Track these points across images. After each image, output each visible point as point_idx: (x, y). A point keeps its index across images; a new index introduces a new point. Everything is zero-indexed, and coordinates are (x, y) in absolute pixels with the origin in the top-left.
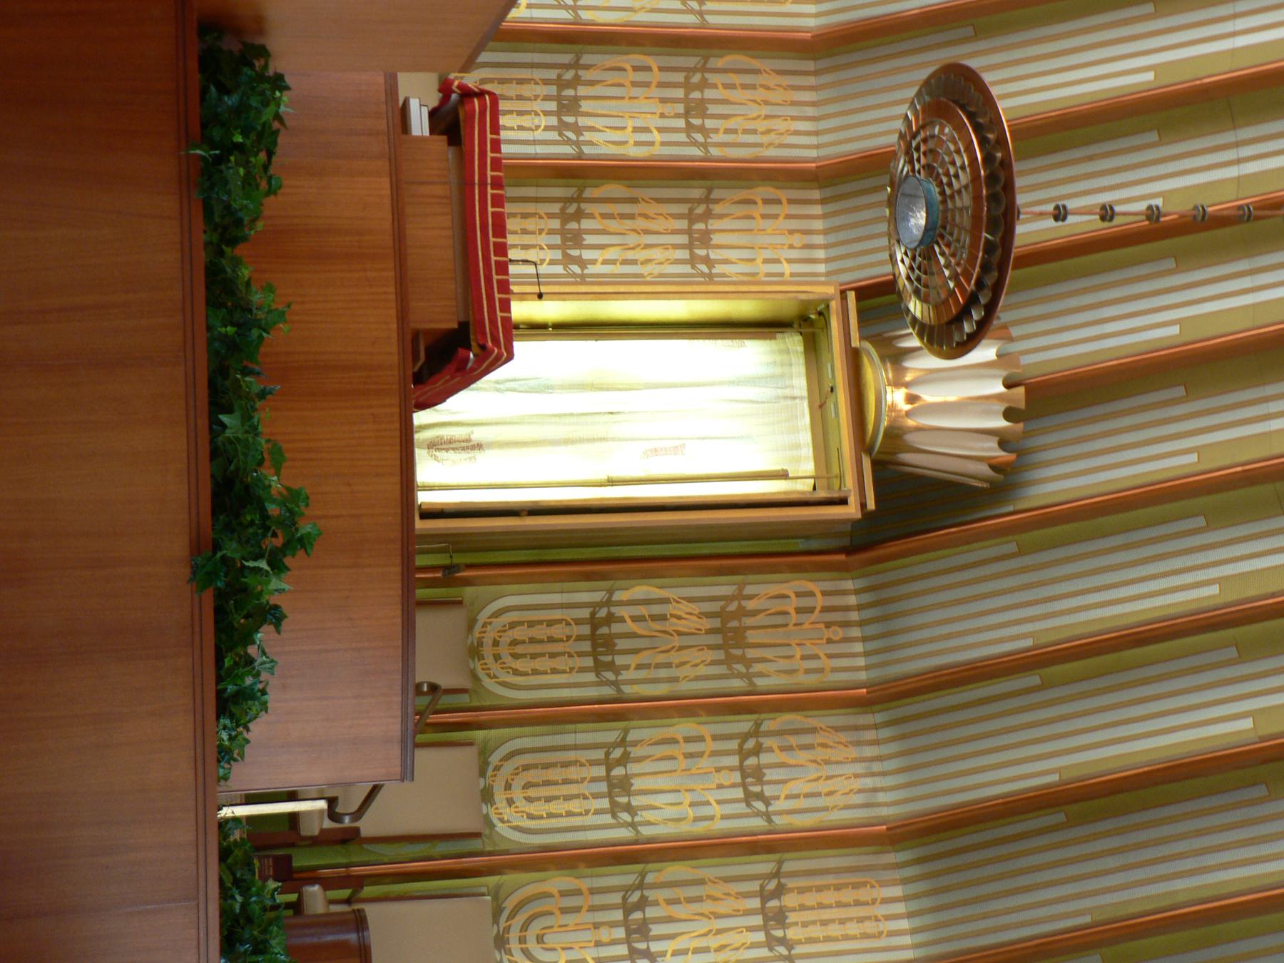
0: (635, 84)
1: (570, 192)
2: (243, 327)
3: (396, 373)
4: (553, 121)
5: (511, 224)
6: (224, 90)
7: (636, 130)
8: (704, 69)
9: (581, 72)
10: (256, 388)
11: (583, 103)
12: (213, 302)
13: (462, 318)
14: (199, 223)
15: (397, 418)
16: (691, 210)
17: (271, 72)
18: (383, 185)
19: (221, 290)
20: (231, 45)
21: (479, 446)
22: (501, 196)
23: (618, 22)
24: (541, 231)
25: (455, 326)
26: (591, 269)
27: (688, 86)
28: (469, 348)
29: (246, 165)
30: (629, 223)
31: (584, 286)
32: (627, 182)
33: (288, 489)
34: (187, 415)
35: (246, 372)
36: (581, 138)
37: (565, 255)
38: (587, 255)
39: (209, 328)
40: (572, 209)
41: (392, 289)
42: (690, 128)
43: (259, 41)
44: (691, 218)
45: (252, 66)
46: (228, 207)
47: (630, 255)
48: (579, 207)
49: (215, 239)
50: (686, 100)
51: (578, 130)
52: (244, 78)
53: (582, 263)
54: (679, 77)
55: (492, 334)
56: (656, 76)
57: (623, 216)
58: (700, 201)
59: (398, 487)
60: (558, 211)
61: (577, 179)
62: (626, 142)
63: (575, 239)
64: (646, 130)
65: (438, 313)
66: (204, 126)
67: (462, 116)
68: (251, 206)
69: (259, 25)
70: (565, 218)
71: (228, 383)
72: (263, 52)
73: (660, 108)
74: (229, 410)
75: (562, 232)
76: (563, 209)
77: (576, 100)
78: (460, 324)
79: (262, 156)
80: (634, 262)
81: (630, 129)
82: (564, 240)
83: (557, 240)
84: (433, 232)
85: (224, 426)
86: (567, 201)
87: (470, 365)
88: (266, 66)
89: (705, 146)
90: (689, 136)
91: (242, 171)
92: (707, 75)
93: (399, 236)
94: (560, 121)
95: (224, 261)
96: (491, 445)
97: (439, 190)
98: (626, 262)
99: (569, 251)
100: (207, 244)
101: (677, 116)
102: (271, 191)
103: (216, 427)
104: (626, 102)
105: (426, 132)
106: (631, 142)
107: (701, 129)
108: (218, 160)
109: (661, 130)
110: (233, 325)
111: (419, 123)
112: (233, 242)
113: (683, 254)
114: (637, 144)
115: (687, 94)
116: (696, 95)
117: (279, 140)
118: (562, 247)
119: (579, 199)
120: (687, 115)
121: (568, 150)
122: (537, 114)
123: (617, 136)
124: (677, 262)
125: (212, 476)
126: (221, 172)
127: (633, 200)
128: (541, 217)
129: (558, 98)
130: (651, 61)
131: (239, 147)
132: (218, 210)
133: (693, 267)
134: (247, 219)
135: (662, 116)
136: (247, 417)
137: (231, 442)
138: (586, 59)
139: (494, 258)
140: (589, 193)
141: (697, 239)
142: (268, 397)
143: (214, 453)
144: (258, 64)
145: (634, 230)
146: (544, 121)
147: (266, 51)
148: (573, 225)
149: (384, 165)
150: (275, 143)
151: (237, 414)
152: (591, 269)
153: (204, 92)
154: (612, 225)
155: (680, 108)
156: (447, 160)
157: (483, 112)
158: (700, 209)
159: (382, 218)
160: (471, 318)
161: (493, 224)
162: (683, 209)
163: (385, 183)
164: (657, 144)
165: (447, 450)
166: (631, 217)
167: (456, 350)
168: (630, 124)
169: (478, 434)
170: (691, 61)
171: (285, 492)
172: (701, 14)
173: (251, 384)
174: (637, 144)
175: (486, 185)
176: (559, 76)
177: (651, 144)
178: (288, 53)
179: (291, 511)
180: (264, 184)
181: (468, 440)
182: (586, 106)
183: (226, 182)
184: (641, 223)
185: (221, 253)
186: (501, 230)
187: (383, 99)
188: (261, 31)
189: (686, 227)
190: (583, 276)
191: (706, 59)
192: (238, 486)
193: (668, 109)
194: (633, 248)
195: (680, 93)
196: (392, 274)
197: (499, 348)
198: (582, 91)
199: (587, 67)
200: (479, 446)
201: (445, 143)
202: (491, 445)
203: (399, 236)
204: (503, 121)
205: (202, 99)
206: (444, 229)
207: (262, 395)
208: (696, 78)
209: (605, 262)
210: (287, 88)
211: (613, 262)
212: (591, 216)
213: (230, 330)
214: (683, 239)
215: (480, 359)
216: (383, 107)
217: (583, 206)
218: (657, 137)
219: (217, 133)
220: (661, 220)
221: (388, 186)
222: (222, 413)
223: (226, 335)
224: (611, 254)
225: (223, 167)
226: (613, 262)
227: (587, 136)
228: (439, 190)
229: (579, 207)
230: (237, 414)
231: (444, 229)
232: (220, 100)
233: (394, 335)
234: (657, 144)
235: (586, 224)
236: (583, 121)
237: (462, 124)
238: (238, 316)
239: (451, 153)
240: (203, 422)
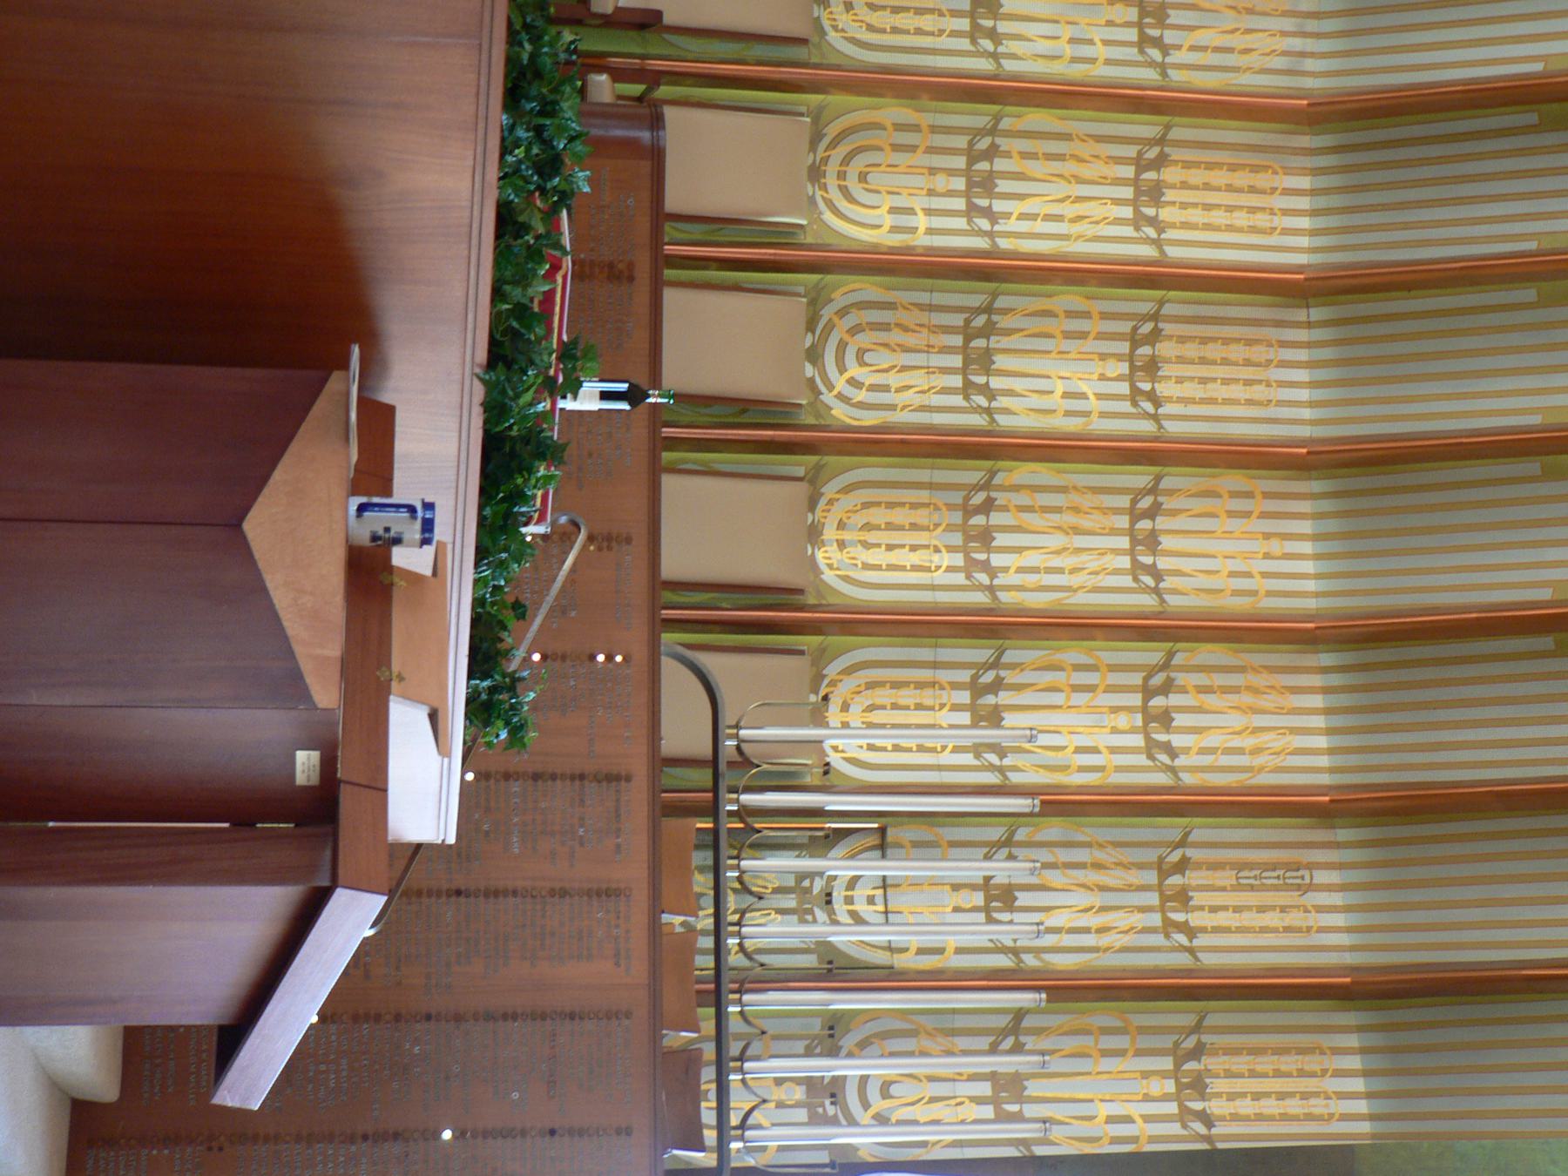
38: (999, 206)
51: (991, 394)
57: (1050, 157)
114: (1068, 413)
174: (1068, 413)
177: (1093, 61)
227: (1003, 402)
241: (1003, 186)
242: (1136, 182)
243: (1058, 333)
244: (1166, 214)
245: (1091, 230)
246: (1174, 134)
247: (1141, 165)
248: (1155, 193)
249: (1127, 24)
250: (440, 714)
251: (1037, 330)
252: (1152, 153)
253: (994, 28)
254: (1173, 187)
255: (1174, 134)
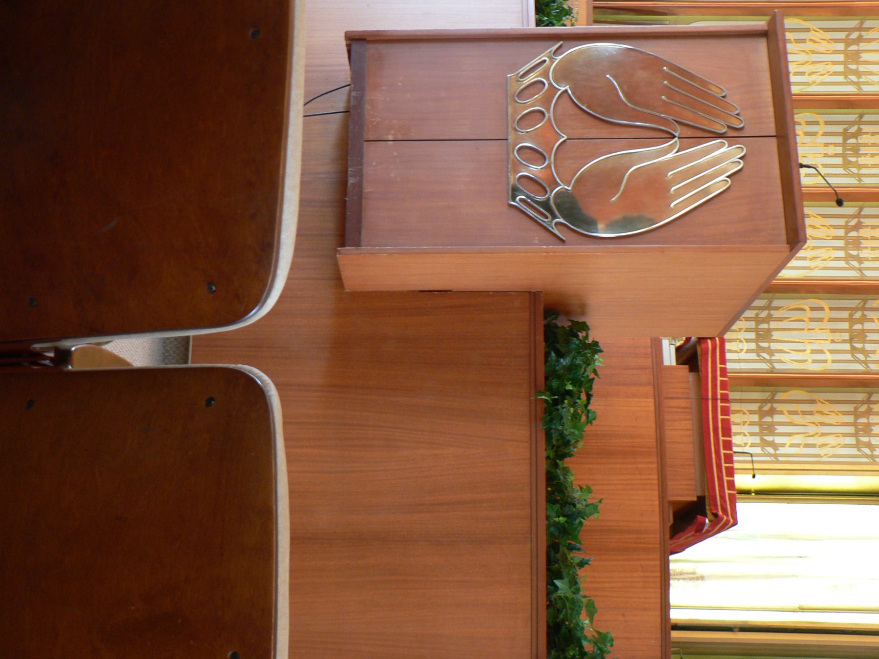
0: (812, 320)
1: (766, 395)
2: (571, 517)
3: (658, 536)
4: (753, 346)
5: (734, 429)
6: (560, 355)
7: (813, 352)
8: (863, 309)
9: (772, 312)
10: (577, 560)
11: (774, 333)
12: (551, 500)
13: (699, 494)
14: (542, 444)
15: (658, 569)
16: (856, 409)
17: (590, 341)
18: (649, 404)
19: (556, 491)
20: (563, 322)
21: (702, 578)
22: (728, 408)
23: (799, 277)
24: (744, 423)
25: (695, 499)
26: (781, 451)
27: (851, 320)
28: (705, 516)
29: (574, 405)
30: (810, 418)
31: (778, 465)
32: (809, 389)
33: (598, 633)
34: (532, 580)
35: (571, 548)
36: (773, 358)
37: (763, 440)
38: (778, 440)
39: (548, 518)
40: (767, 407)
41: (655, 477)
42: (854, 350)
43: (581, 319)
44: (856, 414)
45: (577, 336)
46: (561, 434)
47: (811, 441)
48: (772, 406)
49: (552, 455)
50: (850, 330)
51: (771, 352)
52: (574, 346)
53: (775, 446)
54: (845, 314)
55: (722, 506)
56: (827, 314)
57: (804, 413)
58: (863, 403)
59: (659, 619)
60: (756, 409)
61: (771, 385)
62: (806, 361)
63: (769, 429)
64: (821, 352)
65: (685, 491)
66: (546, 379)
67: (699, 353)
68: (577, 432)
69: (583, 308)
70: (762, 414)
71: (558, 556)
72: (584, 327)
73: (830, 336)
74: (560, 577)
75: (760, 424)
76: (760, 408)
77: (769, 331)
78: (698, 497)
79: (583, 397)
80: (813, 446)
81: (809, 351)
82: (762, 429)
83: (756, 429)
84: (681, 432)
85: (556, 588)
86: (764, 402)
87: (706, 528)
88: (587, 337)
89: (865, 362)
90: (853, 356)
91: (572, 410)
92: (866, 313)
93: (661, 440)
94: (758, 346)
95: (558, 471)
96: (710, 577)
97: (682, 403)
98: (807, 446)
99: (765, 438)
100: (548, 458)
101: (844, 341)
102: (589, 422)
103: (552, 588)
104: (806, 332)
105: (674, 363)
106: (810, 360)
107: (863, 351)
108: (556, 403)
109: (832, 352)
110: (564, 516)
111: (669, 357)
112: (562, 456)
113: (852, 441)
114: (814, 361)
115: (851, 326)
116: (858, 327)
117: (594, 386)
118: (760, 434)
119: (772, 401)
120: (851, 341)
121: (764, 366)
122: (741, 341)
123: (800, 356)
124: (846, 446)
125: (547, 622)
126: (558, 410)
127: (812, 402)
128: (744, 413)
129: (756, 330)
130: (822, 303)
131: (569, 393)
132: (555, 436)
133: (859, 450)
134: (573, 441)
135: (833, 341)
136: (573, 582)
137: (560, 598)
138: (776, 303)
139: (722, 452)
140: (780, 396)
141: (861, 430)
142: (586, 566)
143: (550, 605)
144: (581, 335)
145: (813, 423)
146: (746, 346)
147: (587, 326)
148: (768, 419)
149: (650, 390)
150: (591, 388)
151: (566, 580)
152: (781, 451)
153: (547, 355)
154: (797, 419)
155: (846, 336)
156: (688, 382)
157: (714, 349)
158: (863, 408)
159: (648, 426)
160: (707, 494)
161: (723, 428)
162: (850, 408)
163: (651, 402)
164: (829, 361)
165: (679, 579)
166: (811, 413)
167: (696, 516)
168: (809, 348)
169: (700, 570)
170: (854, 303)
171: (596, 636)
172: (860, 270)
173: (575, 557)
174: (814, 361)
175: (717, 399)
176: (757, 315)
177: (825, 361)
178: (601, 328)
179: (600, 649)
180: (584, 418)
181: (694, 573)
182: (776, 335)
183: (562, 418)
184: (818, 418)
185: (556, 466)
186: (727, 432)
187: (649, 344)
188: (583, 313)
189: (754, 327)
190: (776, 456)
191: (865, 301)
192: (564, 630)
193: (837, 336)
194: (812, 436)
195: (846, 325)
196: (655, 466)
197: (727, 516)
198: (773, 325)
199: (777, 308)
200: (702, 578)
201: (687, 370)
202: (710, 577)
203: (661, 440)
204: (728, 356)
205: (546, 362)
206: (687, 430)
207: (582, 564)
208: (858, 315)
209: (792, 445)
210: (601, 351)
211: (798, 445)
212: (781, 413)
213: (562, 519)
214: (851, 430)
215: (714, 524)
216: (649, 350)
217: (775, 405)
218: (829, 356)
219: (555, 383)
220: (833, 416)
221: (653, 404)
222: (556, 579)
223: (558, 523)
224: (797, 439)
225: (559, 407)
226: (798, 445)
227: (777, 356)
228: (682, 403)
229: (772, 406)
230: (566, 580)
231: (687, 430)
232: (558, 361)
233: (657, 509)
234: (829, 361)
235: (777, 418)
236: (774, 346)
237: (699, 357)
238: (567, 510)
239: (691, 377)
240: (542, 584)
241: (780, 429)
242: (845, 52)
243: (806, 319)
244: (864, 254)
245: (820, 79)
246: (866, 118)
247: (848, 229)
248: (856, 243)
249: (836, 155)
250: (330, 225)
251: (797, 318)
252: (853, 222)
253: (769, 347)
254: (866, 239)
255: (866, 118)
